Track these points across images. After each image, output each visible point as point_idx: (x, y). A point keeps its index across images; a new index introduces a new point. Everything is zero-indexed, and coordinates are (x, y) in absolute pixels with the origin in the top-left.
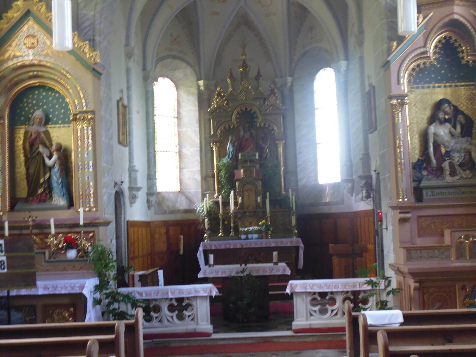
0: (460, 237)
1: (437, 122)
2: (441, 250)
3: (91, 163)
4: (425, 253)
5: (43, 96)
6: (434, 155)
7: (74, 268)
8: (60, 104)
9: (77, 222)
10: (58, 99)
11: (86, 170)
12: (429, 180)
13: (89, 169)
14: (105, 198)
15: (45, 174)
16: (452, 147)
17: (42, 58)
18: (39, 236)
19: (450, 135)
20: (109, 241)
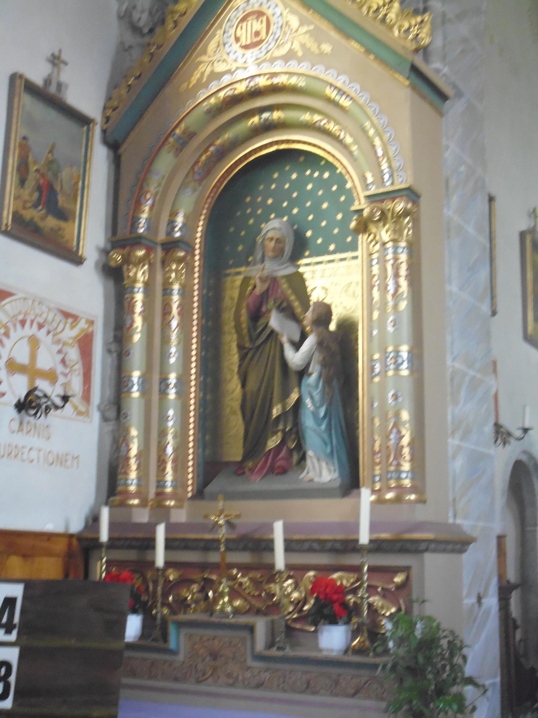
3: (404, 350)
5: (292, 182)
7: (335, 688)
8: (333, 198)
9: (352, 537)
10: (326, 184)
11: (391, 373)
13: (397, 369)
14: (458, 464)
15: (285, 395)
17: (278, 67)
18: (251, 574)
20: (472, 600)
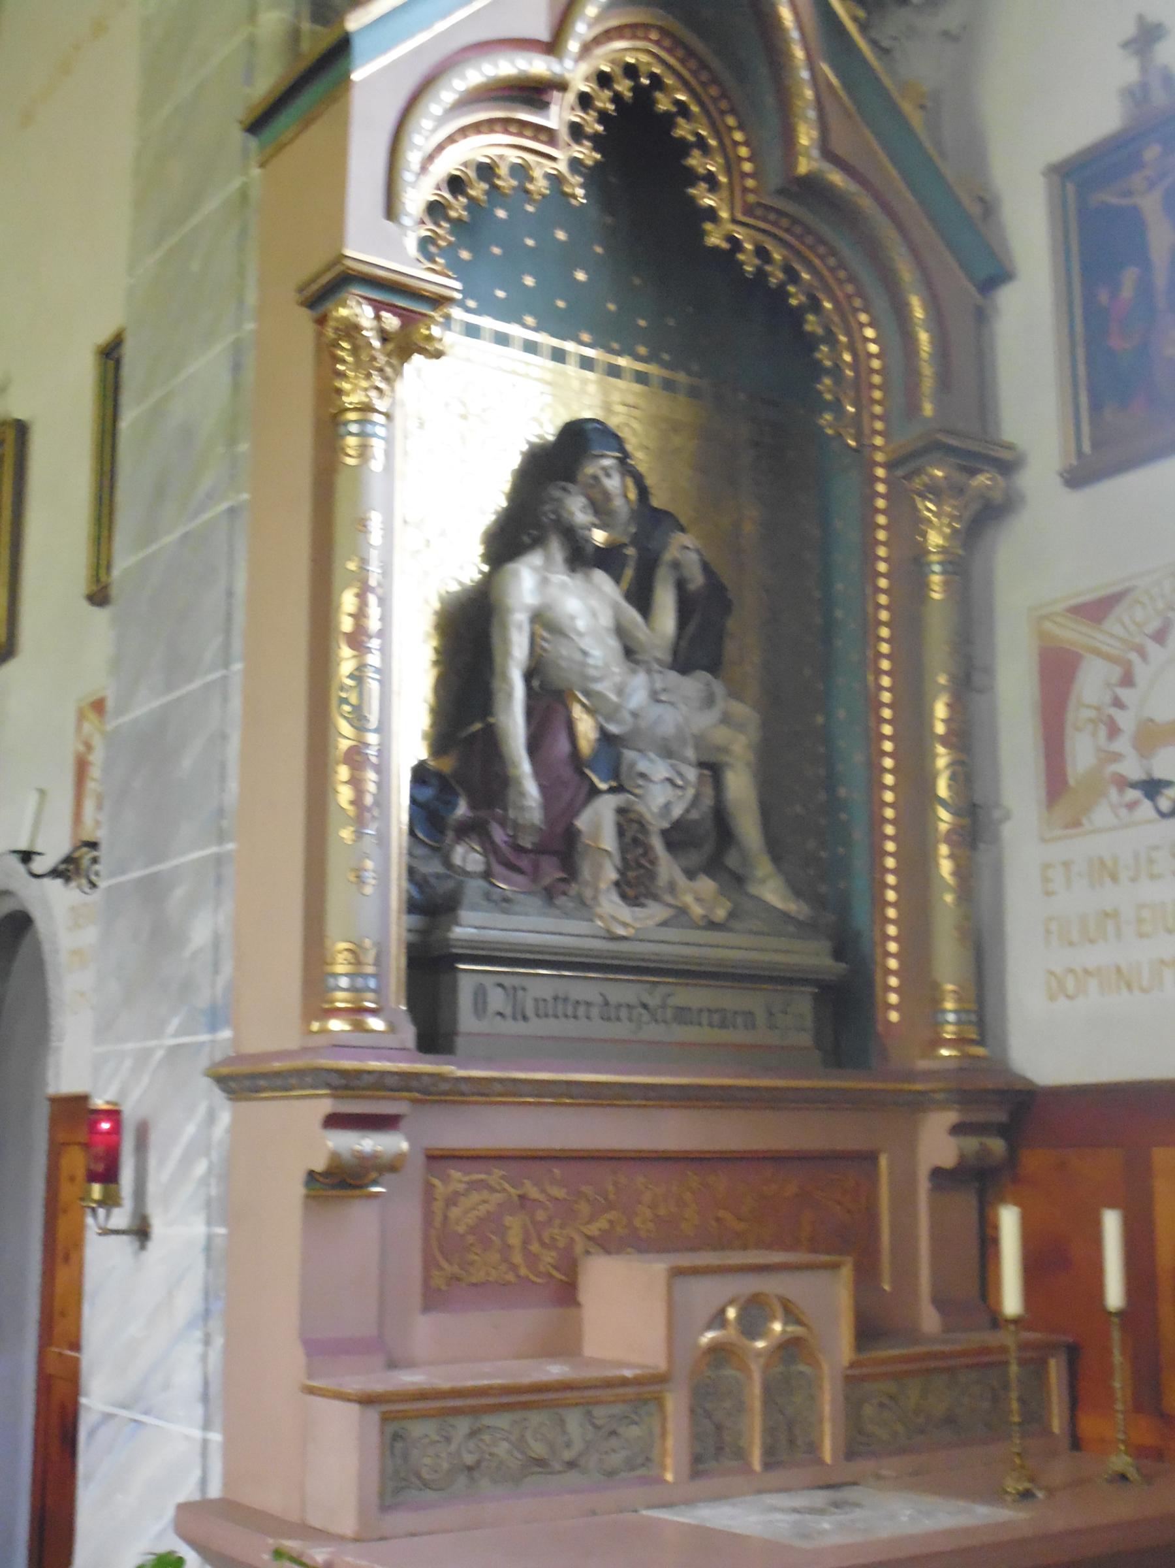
0: (718, 1319)
1: (557, 550)
2: (600, 1412)
4: (502, 1435)
6: (534, 747)
12: (504, 904)
16: (635, 715)
19: (614, 643)
